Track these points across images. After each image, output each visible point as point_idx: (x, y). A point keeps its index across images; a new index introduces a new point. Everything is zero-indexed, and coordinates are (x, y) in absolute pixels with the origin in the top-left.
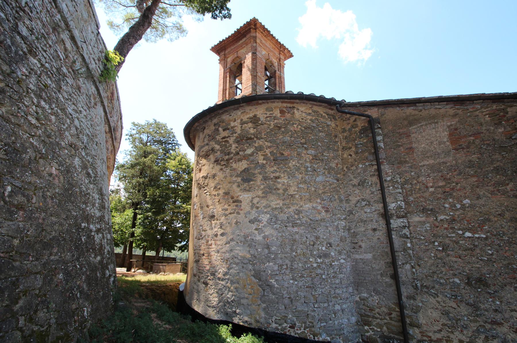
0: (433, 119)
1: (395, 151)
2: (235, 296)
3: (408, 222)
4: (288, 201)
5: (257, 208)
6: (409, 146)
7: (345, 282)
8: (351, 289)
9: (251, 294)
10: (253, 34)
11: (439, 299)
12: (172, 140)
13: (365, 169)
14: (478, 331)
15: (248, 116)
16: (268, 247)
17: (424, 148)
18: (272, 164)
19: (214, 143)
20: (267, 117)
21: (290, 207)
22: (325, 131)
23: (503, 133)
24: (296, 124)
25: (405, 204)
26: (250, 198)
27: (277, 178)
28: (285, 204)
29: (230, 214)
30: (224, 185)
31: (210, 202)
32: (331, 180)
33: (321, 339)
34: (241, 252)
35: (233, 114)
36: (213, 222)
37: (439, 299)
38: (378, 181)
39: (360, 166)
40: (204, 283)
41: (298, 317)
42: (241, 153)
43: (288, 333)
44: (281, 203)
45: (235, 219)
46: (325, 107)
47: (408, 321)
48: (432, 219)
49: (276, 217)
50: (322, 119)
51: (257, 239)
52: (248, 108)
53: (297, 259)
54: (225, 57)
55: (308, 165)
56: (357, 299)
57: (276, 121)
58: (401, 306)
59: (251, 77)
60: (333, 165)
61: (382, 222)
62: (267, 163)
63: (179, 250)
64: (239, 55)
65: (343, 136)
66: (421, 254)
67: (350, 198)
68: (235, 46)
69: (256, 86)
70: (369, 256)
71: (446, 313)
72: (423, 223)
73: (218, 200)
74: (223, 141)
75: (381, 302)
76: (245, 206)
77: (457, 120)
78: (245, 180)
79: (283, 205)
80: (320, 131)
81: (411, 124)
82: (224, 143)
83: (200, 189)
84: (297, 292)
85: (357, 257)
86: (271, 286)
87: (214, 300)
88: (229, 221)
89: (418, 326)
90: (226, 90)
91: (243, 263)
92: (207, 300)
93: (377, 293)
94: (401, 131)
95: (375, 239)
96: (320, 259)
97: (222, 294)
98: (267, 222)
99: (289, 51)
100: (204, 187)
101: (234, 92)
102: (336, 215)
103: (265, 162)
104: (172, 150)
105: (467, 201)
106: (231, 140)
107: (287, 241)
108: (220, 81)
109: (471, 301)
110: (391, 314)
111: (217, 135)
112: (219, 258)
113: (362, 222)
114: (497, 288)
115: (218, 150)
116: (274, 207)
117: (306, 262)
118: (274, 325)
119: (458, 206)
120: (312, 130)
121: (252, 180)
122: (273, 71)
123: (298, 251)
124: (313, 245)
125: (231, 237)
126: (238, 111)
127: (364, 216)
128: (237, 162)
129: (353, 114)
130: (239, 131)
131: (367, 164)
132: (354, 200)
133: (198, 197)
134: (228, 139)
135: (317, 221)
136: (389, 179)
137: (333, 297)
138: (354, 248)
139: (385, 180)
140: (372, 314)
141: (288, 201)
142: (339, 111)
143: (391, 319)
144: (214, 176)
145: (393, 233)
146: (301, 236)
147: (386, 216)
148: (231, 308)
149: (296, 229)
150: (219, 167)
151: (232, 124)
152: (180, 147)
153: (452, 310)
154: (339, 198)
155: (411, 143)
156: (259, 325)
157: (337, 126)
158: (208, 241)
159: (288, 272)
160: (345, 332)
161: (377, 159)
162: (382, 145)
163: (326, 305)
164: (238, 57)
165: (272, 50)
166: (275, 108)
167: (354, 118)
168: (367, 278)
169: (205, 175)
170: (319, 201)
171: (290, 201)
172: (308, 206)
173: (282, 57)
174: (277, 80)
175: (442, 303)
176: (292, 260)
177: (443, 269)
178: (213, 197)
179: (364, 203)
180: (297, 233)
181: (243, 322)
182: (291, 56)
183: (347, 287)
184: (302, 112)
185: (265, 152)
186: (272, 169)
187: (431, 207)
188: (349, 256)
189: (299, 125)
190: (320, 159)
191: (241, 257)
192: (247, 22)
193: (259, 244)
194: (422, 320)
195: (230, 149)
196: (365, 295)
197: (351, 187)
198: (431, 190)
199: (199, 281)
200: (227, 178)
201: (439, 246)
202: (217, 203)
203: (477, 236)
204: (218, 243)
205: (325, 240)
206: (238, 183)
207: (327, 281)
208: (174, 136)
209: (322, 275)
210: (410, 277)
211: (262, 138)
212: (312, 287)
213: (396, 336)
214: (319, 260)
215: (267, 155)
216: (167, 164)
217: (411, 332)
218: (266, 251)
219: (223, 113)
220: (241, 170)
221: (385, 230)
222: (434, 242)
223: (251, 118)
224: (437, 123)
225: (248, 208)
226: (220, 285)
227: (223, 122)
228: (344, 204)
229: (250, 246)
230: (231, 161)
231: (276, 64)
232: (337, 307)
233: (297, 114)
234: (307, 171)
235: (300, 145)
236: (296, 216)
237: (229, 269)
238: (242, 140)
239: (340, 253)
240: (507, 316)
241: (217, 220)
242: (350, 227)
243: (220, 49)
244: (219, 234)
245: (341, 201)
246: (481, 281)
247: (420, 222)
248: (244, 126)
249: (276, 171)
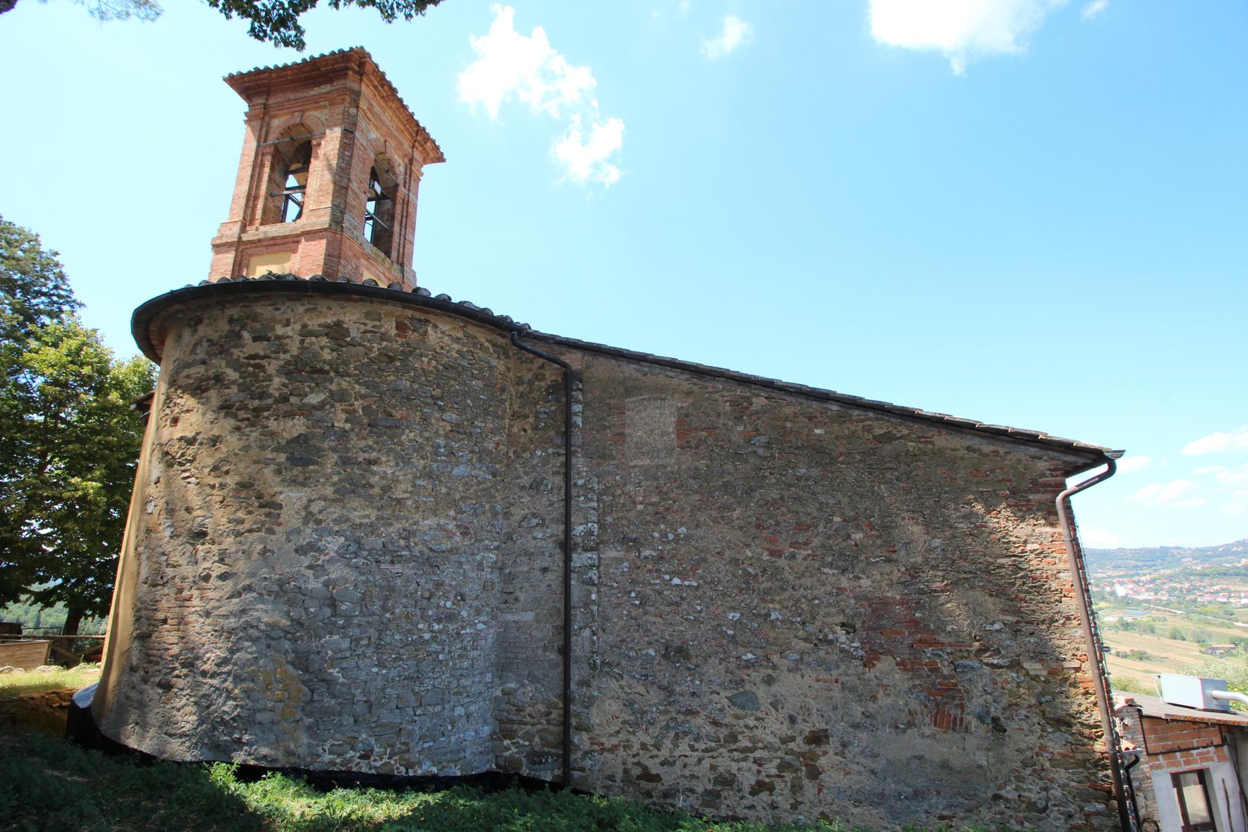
0: (660, 392)
1: (598, 436)
2: (242, 707)
3: (599, 558)
4: (389, 512)
5: (319, 522)
6: (619, 430)
7: (480, 664)
8: (488, 677)
9: (281, 701)
10: (351, 82)
11: (623, 683)
12: (51, 285)
13: (546, 460)
14: (667, 727)
15: (322, 321)
16: (333, 603)
17: (641, 437)
18: (365, 432)
19: (223, 363)
20: (366, 332)
21: (391, 525)
22: (483, 378)
23: (741, 433)
24: (427, 356)
25: (600, 528)
26: (305, 500)
27: (371, 462)
28: (383, 518)
29: (250, 531)
30: (241, 466)
31: (195, 501)
32: (482, 473)
33: (420, 772)
34: (266, 614)
35: (283, 308)
36: (200, 547)
37: (623, 683)
38: (563, 484)
39: (539, 453)
40: (160, 685)
41: (378, 737)
42: (293, 400)
43: (354, 769)
44: (373, 514)
45: (261, 543)
46: (491, 331)
47: (574, 722)
48: (634, 554)
49: (358, 542)
50: (481, 354)
51: (310, 587)
52: (323, 304)
53: (391, 626)
54: (265, 114)
55: (441, 441)
56: (499, 693)
57: (385, 343)
58: (566, 698)
59: (331, 187)
60: (491, 446)
61: (559, 557)
62: (352, 430)
63: (35, 602)
64: (308, 122)
65: (517, 391)
66: (609, 611)
67: (512, 510)
68: (298, 95)
69: (343, 213)
70: (529, 616)
71: (629, 704)
72: (620, 561)
73: (220, 499)
74: (249, 365)
75: (535, 695)
76: (290, 517)
77: (690, 401)
78: (293, 461)
79: (377, 518)
80: (473, 377)
81: (628, 393)
82: (251, 369)
83: (170, 465)
84: (383, 689)
85: (509, 617)
86: (329, 682)
87: (187, 719)
88: (245, 547)
89: (588, 729)
90: (256, 198)
91: (270, 637)
92: (167, 722)
93: (533, 678)
94: (612, 402)
95: (543, 587)
96: (438, 623)
97: (208, 707)
98: (336, 552)
99: (437, 148)
100: (181, 464)
101: (279, 208)
102: (481, 541)
103: (348, 426)
104: (50, 314)
105: (682, 530)
106: (272, 367)
107: (376, 591)
108: (241, 169)
109: (665, 683)
110: (549, 714)
111: (236, 346)
112: (209, 628)
113: (526, 554)
114: (700, 660)
115: (234, 382)
116: (358, 521)
117: (409, 631)
118: (327, 757)
119: (671, 536)
120: (459, 374)
121: (316, 463)
122: (391, 184)
123: (397, 611)
124: (429, 599)
125: (247, 582)
126: (298, 304)
127: (531, 545)
128: (281, 419)
129: (540, 356)
130: (294, 349)
131: (550, 451)
132: (518, 513)
133: (161, 486)
134: (264, 362)
135: (443, 552)
136: (580, 482)
137: (454, 694)
138: (506, 602)
139: (575, 484)
140: (519, 718)
141: (389, 512)
142: (514, 343)
143: (548, 722)
144: (215, 441)
145: (573, 575)
146: (408, 581)
147: (567, 546)
148: (230, 734)
149: (398, 568)
150: (232, 422)
151: (280, 330)
152: (79, 312)
153: (638, 698)
154: (493, 509)
155: (624, 426)
156: (293, 760)
157: (509, 369)
158: (181, 591)
159: (369, 652)
160: (467, 755)
161: (568, 445)
162: (579, 420)
163: (438, 709)
164: (303, 125)
165: (396, 133)
166: (387, 315)
167: (541, 361)
168: (520, 656)
169: (190, 435)
170: (452, 513)
171: (394, 511)
172: (431, 521)
173: (418, 156)
174: (399, 207)
175: (627, 689)
176: (383, 628)
177: (636, 635)
178: (208, 490)
179: (534, 521)
180: (400, 575)
181: (256, 759)
182: (440, 158)
183: (481, 674)
184: (440, 334)
185: (352, 405)
186: (362, 444)
187: (634, 536)
188: (494, 617)
189: (434, 358)
190: (465, 433)
191: (267, 624)
192: (341, 51)
193: (312, 598)
194: (595, 718)
195: (268, 386)
196: (513, 685)
197: (517, 490)
198: (640, 507)
199: (145, 681)
200: (252, 452)
201: (636, 598)
202: (217, 506)
203: (687, 583)
204: (211, 594)
205: (454, 587)
206: (277, 464)
207: (447, 665)
208: (62, 276)
209: (437, 653)
210: (587, 649)
211: (348, 375)
212: (416, 678)
213: (553, 751)
214: (436, 627)
215: (355, 411)
216: (27, 356)
217: (576, 740)
218: (328, 611)
219: (257, 300)
220: (287, 436)
221: (561, 572)
222: (630, 592)
223: (327, 326)
224: (664, 399)
225: (296, 522)
226: (207, 687)
227: (255, 318)
228: (500, 521)
229: (291, 603)
230: (266, 414)
231: (402, 169)
232: (460, 711)
233: (433, 336)
234: (436, 454)
235: (429, 401)
236: (402, 542)
237: (232, 651)
238: (299, 371)
239: (478, 612)
240: (705, 700)
241: (214, 543)
242: (503, 563)
243: (251, 85)
244: (214, 574)
245: (495, 514)
246: (682, 652)
247: (616, 558)
248: (308, 340)
249: (371, 447)
